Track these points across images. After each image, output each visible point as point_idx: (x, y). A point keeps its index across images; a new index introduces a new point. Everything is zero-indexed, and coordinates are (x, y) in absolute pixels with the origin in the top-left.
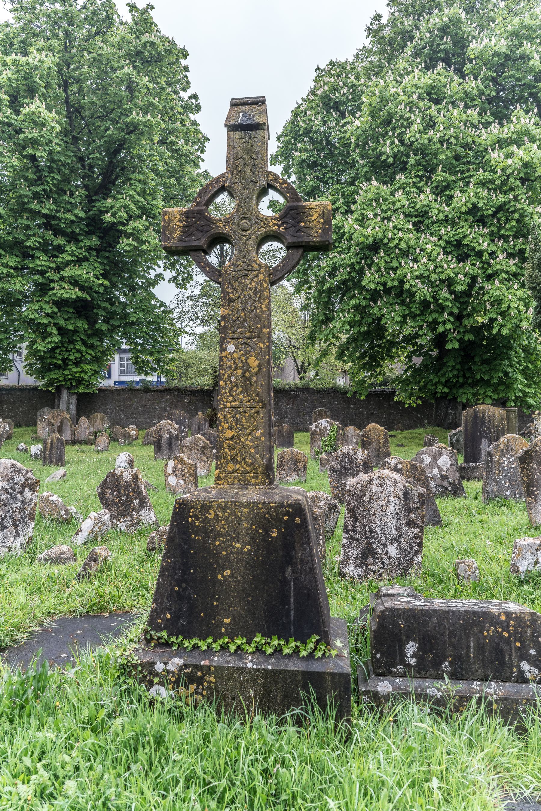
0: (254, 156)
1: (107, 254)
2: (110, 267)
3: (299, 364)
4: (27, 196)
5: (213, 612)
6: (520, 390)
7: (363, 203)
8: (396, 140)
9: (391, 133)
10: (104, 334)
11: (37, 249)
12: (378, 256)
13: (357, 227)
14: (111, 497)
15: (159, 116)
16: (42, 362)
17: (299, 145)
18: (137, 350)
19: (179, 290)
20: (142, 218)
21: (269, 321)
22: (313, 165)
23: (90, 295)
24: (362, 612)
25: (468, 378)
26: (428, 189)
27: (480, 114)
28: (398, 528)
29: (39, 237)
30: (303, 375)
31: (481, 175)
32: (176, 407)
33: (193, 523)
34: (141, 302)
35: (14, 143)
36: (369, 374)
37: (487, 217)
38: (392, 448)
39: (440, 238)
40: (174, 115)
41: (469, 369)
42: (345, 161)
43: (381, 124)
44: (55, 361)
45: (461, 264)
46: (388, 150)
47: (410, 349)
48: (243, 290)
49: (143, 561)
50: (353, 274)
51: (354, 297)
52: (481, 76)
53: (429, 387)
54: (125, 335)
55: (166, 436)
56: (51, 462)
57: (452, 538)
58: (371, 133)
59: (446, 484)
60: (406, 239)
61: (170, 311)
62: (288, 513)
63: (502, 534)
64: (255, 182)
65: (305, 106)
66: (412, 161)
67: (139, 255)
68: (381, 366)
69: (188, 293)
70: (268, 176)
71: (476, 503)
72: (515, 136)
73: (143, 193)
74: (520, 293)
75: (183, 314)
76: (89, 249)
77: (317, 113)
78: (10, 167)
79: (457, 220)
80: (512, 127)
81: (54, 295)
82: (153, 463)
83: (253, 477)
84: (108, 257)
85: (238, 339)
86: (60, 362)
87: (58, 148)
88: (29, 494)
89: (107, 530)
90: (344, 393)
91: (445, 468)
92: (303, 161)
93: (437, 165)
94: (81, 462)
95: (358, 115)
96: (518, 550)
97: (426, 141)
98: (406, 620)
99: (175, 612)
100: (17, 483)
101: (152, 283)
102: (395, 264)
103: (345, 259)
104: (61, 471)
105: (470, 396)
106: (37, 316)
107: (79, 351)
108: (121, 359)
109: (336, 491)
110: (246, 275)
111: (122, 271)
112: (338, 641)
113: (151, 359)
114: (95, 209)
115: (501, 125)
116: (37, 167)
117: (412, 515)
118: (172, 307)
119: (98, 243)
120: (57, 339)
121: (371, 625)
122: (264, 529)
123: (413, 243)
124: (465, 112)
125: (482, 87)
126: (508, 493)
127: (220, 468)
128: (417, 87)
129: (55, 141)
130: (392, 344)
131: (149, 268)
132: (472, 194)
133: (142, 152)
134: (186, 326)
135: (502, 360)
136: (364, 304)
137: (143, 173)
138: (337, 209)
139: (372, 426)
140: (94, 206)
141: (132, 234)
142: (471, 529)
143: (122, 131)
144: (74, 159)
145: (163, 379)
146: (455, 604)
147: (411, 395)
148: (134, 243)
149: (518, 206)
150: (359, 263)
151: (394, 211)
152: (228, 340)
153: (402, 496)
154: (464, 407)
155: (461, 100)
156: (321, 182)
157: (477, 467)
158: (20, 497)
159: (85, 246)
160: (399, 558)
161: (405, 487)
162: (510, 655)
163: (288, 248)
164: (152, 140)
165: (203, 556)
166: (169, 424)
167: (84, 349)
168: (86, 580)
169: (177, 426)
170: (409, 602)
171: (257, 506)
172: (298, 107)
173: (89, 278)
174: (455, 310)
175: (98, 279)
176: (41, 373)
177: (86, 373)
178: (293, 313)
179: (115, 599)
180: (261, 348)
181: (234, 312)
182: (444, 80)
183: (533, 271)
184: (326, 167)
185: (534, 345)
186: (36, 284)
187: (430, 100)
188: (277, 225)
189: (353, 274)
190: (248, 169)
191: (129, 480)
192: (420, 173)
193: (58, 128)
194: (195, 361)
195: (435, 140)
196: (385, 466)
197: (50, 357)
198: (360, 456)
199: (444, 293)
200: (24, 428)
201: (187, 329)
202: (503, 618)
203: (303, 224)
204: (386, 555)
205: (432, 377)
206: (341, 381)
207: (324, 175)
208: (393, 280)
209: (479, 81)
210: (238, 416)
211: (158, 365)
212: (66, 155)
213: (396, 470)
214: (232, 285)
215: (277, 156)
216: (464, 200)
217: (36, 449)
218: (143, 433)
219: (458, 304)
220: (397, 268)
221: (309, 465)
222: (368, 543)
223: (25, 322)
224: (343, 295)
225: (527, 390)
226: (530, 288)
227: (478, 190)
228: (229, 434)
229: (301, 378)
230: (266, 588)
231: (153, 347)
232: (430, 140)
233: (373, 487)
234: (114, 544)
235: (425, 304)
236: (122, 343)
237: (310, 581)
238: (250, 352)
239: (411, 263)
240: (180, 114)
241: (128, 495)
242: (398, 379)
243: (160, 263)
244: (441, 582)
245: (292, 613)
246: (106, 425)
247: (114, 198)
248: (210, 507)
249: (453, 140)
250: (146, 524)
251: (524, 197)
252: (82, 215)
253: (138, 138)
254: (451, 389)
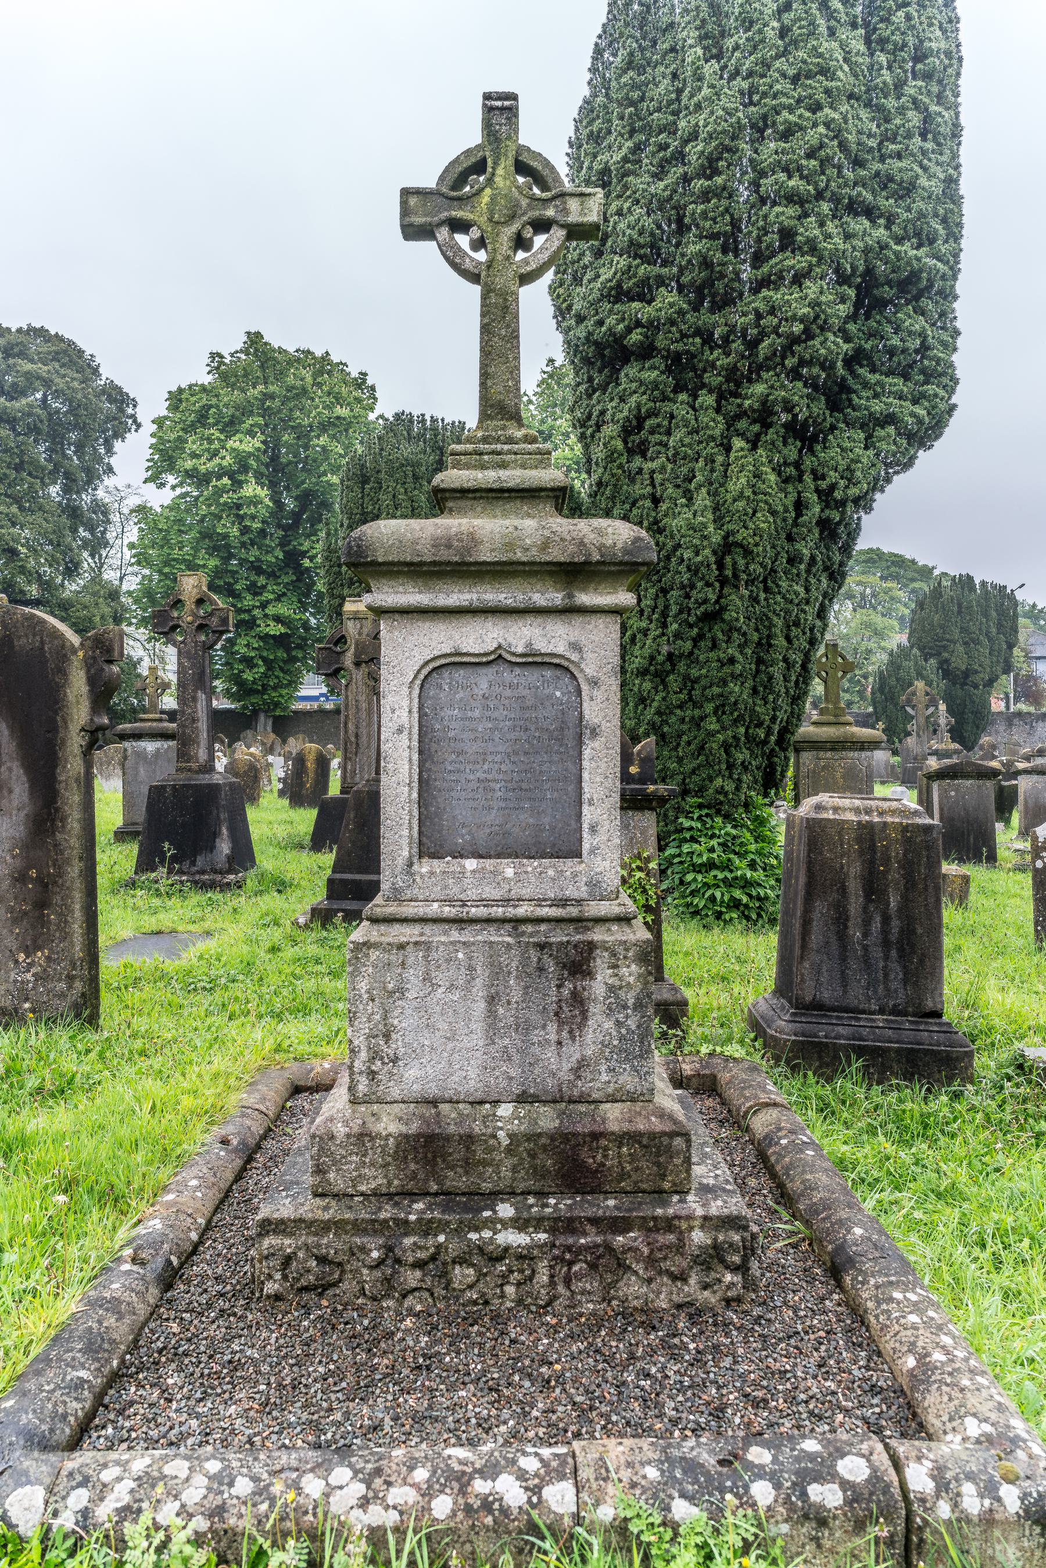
107: (277, 677)
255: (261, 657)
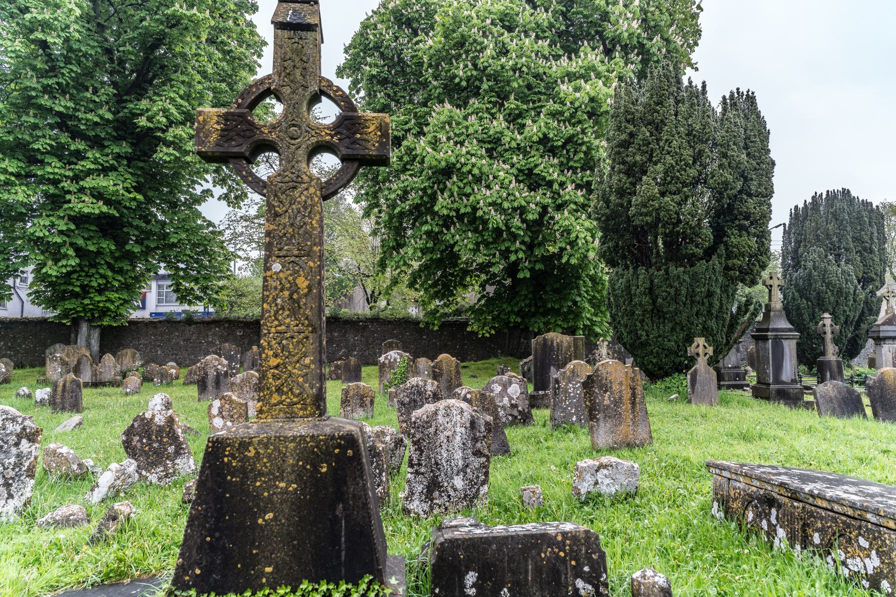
0: (305, 58)
1: (141, 164)
2: (144, 178)
3: (369, 292)
4: (34, 89)
5: (252, 562)
6: (588, 319)
7: (436, 125)
8: (470, 64)
9: (464, 56)
10: (136, 257)
11: (48, 153)
12: (451, 181)
13: (430, 150)
14: (139, 445)
15: (208, 11)
16: (53, 289)
17: (368, 59)
18: (179, 276)
19: (231, 209)
20: (185, 125)
21: (321, 238)
22: (384, 82)
23: (118, 211)
24: (423, 548)
25: (539, 307)
26: (501, 116)
27: (550, 46)
28: (464, 459)
29: (50, 138)
30: (373, 304)
31: (551, 106)
32: (226, 341)
33: (230, 462)
34: (183, 220)
35: (18, 24)
36: (442, 303)
37: (557, 147)
38: (464, 379)
39: (513, 166)
40: (225, 12)
41: (541, 298)
42: (418, 81)
43: (454, 45)
44: (71, 288)
45: (532, 193)
46: (461, 73)
47: (484, 277)
48: (291, 204)
49: (176, 516)
50: (425, 199)
51: (426, 222)
52: (552, 9)
53: (502, 316)
54: (163, 258)
55: (212, 373)
56: (63, 409)
57: (519, 466)
58: (444, 54)
59: (515, 413)
60: (479, 165)
61: (220, 232)
62: (339, 446)
63: (567, 459)
64: (305, 87)
65: (376, 19)
66: (485, 86)
67: (181, 167)
68: (454, 295)
69: (241, 213)
70: (320, 81)
71: (544, 430)
72: (582, 71)
73: (187, 97)
74: (587, 224)
75: (235, 236)
76: (118, 157)
77: (388, 28)
78: (11, 51)
79: (528, 149)
80: (580, 62)
81: (71, 209)
82: (196, 405)
83: (301, 409)
84: (142, 168)
85: (285, 257)
86: (77, 289)
87: (77, 35)
88: (28, 445)
89: (133, 483)
90: (416, 323)
91: (515, 397)
92: (373, 76)
93: (510, 93)
94: (104, 407)
95: (431, 34)
96: (580, 473)
97: (499, 68)
98: (466, 549)
99: (206, 566)
100: (11, 433)
101: (198, 200)
102: (468, 190)
103: (417, 182)
104: (77, 418)
105: (542, 326)
106: (47, 233)
107: (103, 276)
108: (159, 287)
109: (404, 425)
110: (295, 188)
111: (161, 184)
112: (393, 578)
113: (196, 288)
114: (126, 111)
115: (570, 59)
116: (49, 55)
117: (479, 445)
118: (222, 228)
119: (130, 151)
120: (74, 262)
121: (430, 560)
122: (312, 465)
123: (486, 169)
124: (536, 43)
125: (552, 20)
126: (574, 419)
127: (263, 401)
128: (490, 13)
129: (74, 26)
130: (466, 272)
131: (194, 182)
132: (542, 124)
133: (187, 50)
134: (239, 249)
135: (571, 289)
136: (437, 230)
137: (188, 75)
138: (409, 130)
139: (443, 356)
140: (125, 108)
141: (173, 143)
142: (538, 456)
143: (162, 23)
144: (99, 50)
145: (211, 310)
146: (516, 529)
147: (485, 325)
148: (175, 152)
149: (586, 139)
150: (432, 188)
151: (468, 136)
152: (274, 258)
153: (468, 425)
154: (536, 335)
155: (533, 30)
156: (392, 100)
157: (546, 395)
158: (14, 450)
159: (112, 153)
160: (465, 490)
161: (472, 416)
162: (566, 574)
163: (343, 160)
164: (199, 38)
165: (241, 499)
166: (216, 359)
167: (110, 274)
168: (102, 543)
169: (225, 362)
170: (470, 531)
171: (305, 440)
172: (368, 19)
173: (117, 191)
174: (527, 239)
175: (130, 192)
176: (51, 303)
177: (112, 302)
178: (362, 239)
179: (138, 562)
180: (311, 268)
181: (282, 227)
182: (516, 9)
183: (598, 201)
184: (397, 84)
185: (600, 274)
186: (46, 194)
187: (503, 27)
188: (330, 134)
189: (425, 199)
190: (298, 72)
191: (162, 424)
192: (493, 99)
193: (78, 12)
194: (251, 289)
195: (507, 68)
196: (456, 396)
197: (65, 283)
198: (429, 388)
199: (516, 222)
200: (28, 370)
201: (240, 253)
202: (559, 538)
203: (358, 136)
204: (452, 487)
205: (505, 306)
206: (413, 311)
207: (395, 93)
208: (466, 206)
209: (550, 14)
210: (284, 342)
211: (205, 293)
212: (89, 45)
213: (465, 399)
214: (279, 198)
215: (344, 68)
216: (535, 130)
217: (43, 393)
218: (184, 372)
219: (529, 233)
220: (470, 194)
221: (376, 400)
222: (434, 476)
223: (30, 240)
224: (415, 220)
225: (594, 319)
226: (596, 219)
227: (549, 121)
228: (274, 362)
229: (371, 308)
230: (314, 529)
231: (199, 272)
232: (503, 67)
233: (439, 417)
234: (141, 500)
235: (498, 231)
236: (160, 267)
237: (364, 517)
238: (298, 271)
239: (483, 190)
240: (233, 11)
241: (160, 442)
242: (471, 308)
243: (208, 177)
244: (507, 510)
245: (343, 553)
246: (138, 363)
247: (151, 100)
248: (250, 444)
249: (524, 69)
250: (183, 473)
251: (591, 130)
252: (109, 116)
253: (181, 34)
254: (523, 318)
255: (72, 245)
